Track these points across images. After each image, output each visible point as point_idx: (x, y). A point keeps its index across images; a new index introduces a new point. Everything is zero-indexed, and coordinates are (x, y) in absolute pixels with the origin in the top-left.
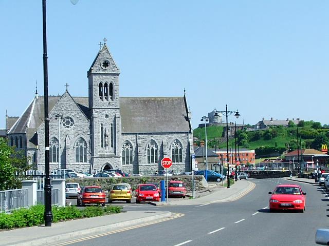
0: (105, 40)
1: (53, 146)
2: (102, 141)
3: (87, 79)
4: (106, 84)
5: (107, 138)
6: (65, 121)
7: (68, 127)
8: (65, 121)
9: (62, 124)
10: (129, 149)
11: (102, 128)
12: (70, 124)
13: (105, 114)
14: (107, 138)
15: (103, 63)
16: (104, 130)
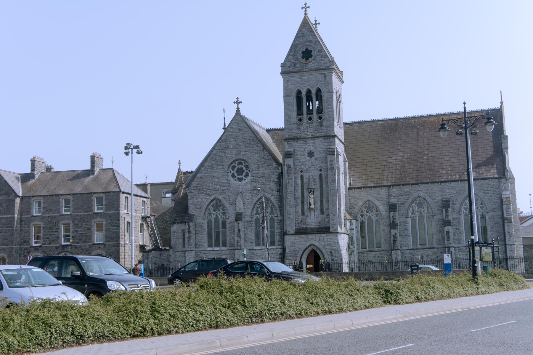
0: (238, 102)
1: (214, 217)
2: (303, 202)
3: (281, 78)
4: (309, 92)
5: (312, 196)
6: (236, 169)
7: (240, 180)
8: (236, 169)
9: (230, 174)
10: (374, 217)
11: (302, 177)
12: (244, 169)
13: (307, 150)
14: (312, 196)
15: (303, 52)
16: (305, 181)
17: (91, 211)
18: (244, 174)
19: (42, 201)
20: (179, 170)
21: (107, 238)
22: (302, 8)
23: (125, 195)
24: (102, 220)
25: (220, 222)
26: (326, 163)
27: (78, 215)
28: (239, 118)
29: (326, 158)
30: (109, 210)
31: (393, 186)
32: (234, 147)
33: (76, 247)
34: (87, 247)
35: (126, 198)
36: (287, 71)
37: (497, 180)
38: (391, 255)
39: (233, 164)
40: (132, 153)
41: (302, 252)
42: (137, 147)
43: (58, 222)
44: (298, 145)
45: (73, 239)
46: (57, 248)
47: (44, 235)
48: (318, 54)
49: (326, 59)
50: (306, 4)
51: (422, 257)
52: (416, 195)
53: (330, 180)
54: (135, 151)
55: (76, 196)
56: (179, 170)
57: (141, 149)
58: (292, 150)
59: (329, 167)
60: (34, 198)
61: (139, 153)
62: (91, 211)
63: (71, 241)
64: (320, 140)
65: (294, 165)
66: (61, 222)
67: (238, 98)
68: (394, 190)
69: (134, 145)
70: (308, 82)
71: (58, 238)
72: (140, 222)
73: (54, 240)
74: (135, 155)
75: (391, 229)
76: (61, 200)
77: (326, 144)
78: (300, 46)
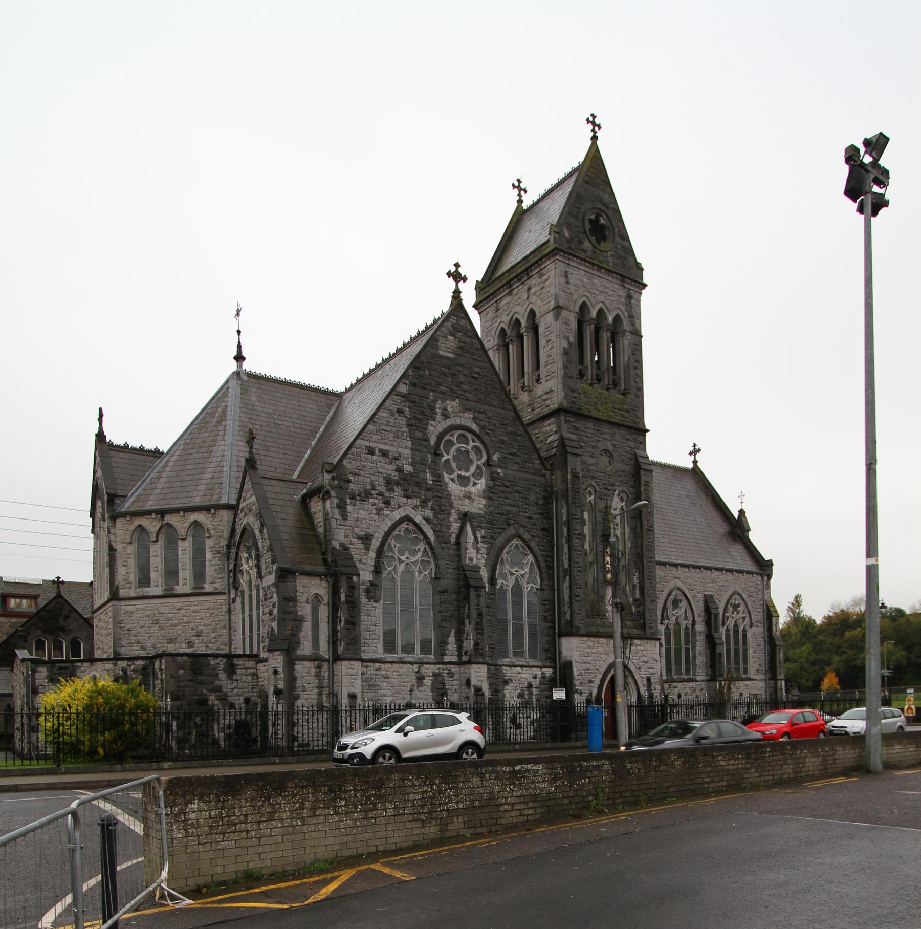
18: (473, 469)
20: (100, 437)
32: (451, 390)
41: (600, 676)
51: (679, 696)
56: (100, 437)
64: (622, 431)
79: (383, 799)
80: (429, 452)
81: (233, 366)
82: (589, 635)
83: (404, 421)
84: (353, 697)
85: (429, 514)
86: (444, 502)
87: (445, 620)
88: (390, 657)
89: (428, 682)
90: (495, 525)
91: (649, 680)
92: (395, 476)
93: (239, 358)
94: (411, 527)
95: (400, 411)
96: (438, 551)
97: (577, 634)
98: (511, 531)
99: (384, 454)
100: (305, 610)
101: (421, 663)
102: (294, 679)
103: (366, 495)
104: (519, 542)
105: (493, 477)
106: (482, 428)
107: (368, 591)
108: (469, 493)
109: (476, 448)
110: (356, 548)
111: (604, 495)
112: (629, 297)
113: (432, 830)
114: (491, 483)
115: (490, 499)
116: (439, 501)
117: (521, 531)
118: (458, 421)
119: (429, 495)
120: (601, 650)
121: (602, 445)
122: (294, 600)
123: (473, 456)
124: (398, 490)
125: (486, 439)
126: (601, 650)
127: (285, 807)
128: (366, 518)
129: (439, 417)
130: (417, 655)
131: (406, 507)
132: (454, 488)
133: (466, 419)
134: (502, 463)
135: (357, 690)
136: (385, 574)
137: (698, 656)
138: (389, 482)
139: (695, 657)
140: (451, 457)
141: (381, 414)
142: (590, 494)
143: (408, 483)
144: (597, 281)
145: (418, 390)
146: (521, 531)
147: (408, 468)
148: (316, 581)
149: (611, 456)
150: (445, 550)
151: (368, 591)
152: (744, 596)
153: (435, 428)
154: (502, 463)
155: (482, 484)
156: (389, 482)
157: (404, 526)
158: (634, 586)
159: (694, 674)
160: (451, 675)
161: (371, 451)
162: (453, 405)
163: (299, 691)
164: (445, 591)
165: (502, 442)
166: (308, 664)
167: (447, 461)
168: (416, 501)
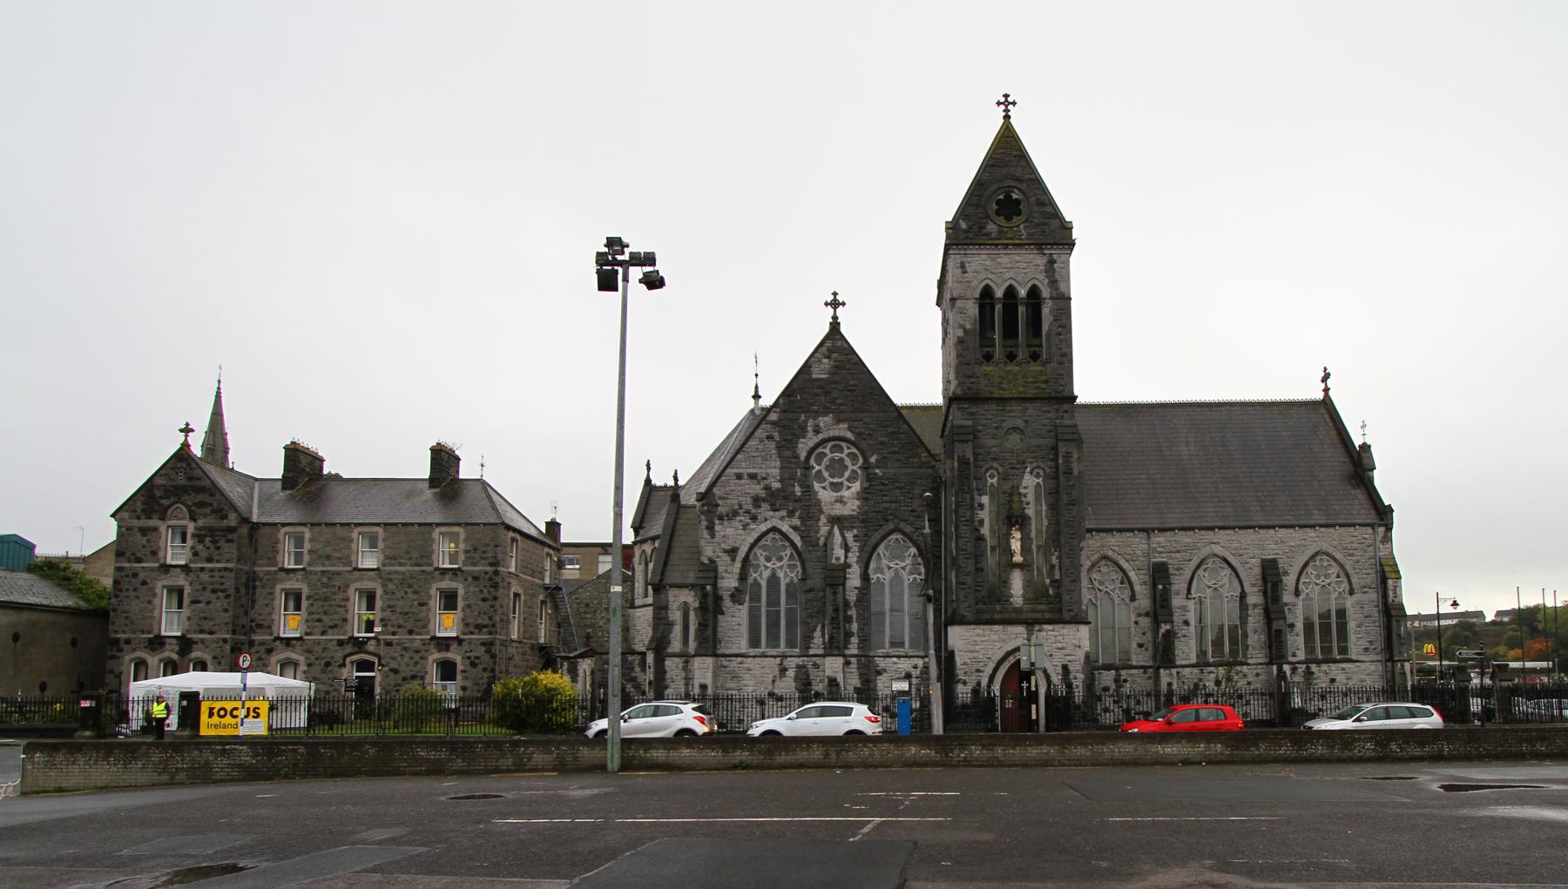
0: (835, 304)
1: (766, 574)
6: (825, 461)
17: (430, 565)
18: (847, 474)
19: (307, 535)
20: (648, 481)
21: (467, 625)
22: (999, 103)
23: (511, 534)
24: (454, 585)
25: (783, 587)
26: (1056, 459)
27: (396, 572)
28: (835, 344)
29: (1055, 448)
30: (473, 564)
31: (1160, 530)
33: (389, 644)
34: (417, 644)
35: (513, 540)
36: (964, 234)
37: (1369, 530)
38: (1157, 678)
39: (820, 450)
40: (626, 279)
41: (992, 665)
42: (649, 259)
43: (347, 586)
44: (987, 412)
45: (384, 626)
46: (341, 643)
47: (310, 614)
48: (1036, 208)
49: (1056, 223)
50: (1006, 96)
52: (1205, 551)
53: (1065, 498)
54: (636, 273)
55: (394, 528)
56: (648, 481)
57: (661, 267)
58: (970, 423)
59: (1061, 469)
60: (288, 529)
61: (654, 282)
62: (430, 565)
63: (378, 629)
65: (976, 460)
66: (353, 587)
67: (835, 294)
68: (1159, 539)
69: (633, 248)
70: (1014, 269)
71: (345, 620)
72: (541, 597)
73: (336, 626)
74: (636, 289)
75: (164, 720)
76: (355, 535)
77: (1052, 415)
78: (993, 188)
79: (136, 759)
80: (797, 469)
81: (751, 404)
82: (978, 622)
83: (772, 445)
84: (704, 687)
85: (796, 522)
86: (813, 509)
87: (810, 616)
88: (752, 651)
89: (791, 673)
90: (871, 526)
91: (1065, 668)
92: (763, 494)
93: (757, 396)
94: (777, 536)
95: (770, 437)
96: (805, 556)
97: (962, 622)
98: (891, 526)
99: (753, 476)
100: (676, 615)
101: (784, 656)
102: (951, 655)
103: (734, 514)
104: (900, 536)
105: (870, 478)
106: (859, 435)
107: (732, 596)
108: (840, 496)
109: (850, 455)
110: (723, 561)
111: (1011, 474)
112: (1052, 262)
113: (165, 778)
114: (866, 485)
115: (865, 499)
116: (808, 508)
117: (902, 525)
118: (831, 434)
119: (798, 505)
120: (994, 637)
121: (1007, 424)
122: (666, 608)
123: (848, 462)
124: (765, 506)
125: (863, 444)
126: (994, 637)
127: (81, 759)
128: (734, 534)
129: (810, 434)
130: (782, 648)
131: (777, 520)
132: (825, 495)
133: (842, 430)
134: (879, 464)
135: (708, 681)
136: (750, 580)
137: (1250, 634)
138: (757, 501)
139: (1245, 636)
140: (822, 468)
141: (752, 443)
142: (992, 477)
143: (775, 499)
144: (1005, 260)
145: (790, 415)
146: (902, 525)
147: (776, 485)
148: (686, 591)
149: (1022, 432)
150: (810, 551)
151: (732, 596)
152: (1338, 556)
153: (803, 447)
154: (879, 464)
155: (856, 486)
156: (757, 501)
157: (771, 535)
158: (1053, 567)
159: (1245, 655)
160: (816, 666)
161: (739, 477)
162: (824, 421)
163: (668, 682)
164: (810, 591)
165: (882, 443)
166: (677, 660)
167: (819, 472)
168: (784, 513)
